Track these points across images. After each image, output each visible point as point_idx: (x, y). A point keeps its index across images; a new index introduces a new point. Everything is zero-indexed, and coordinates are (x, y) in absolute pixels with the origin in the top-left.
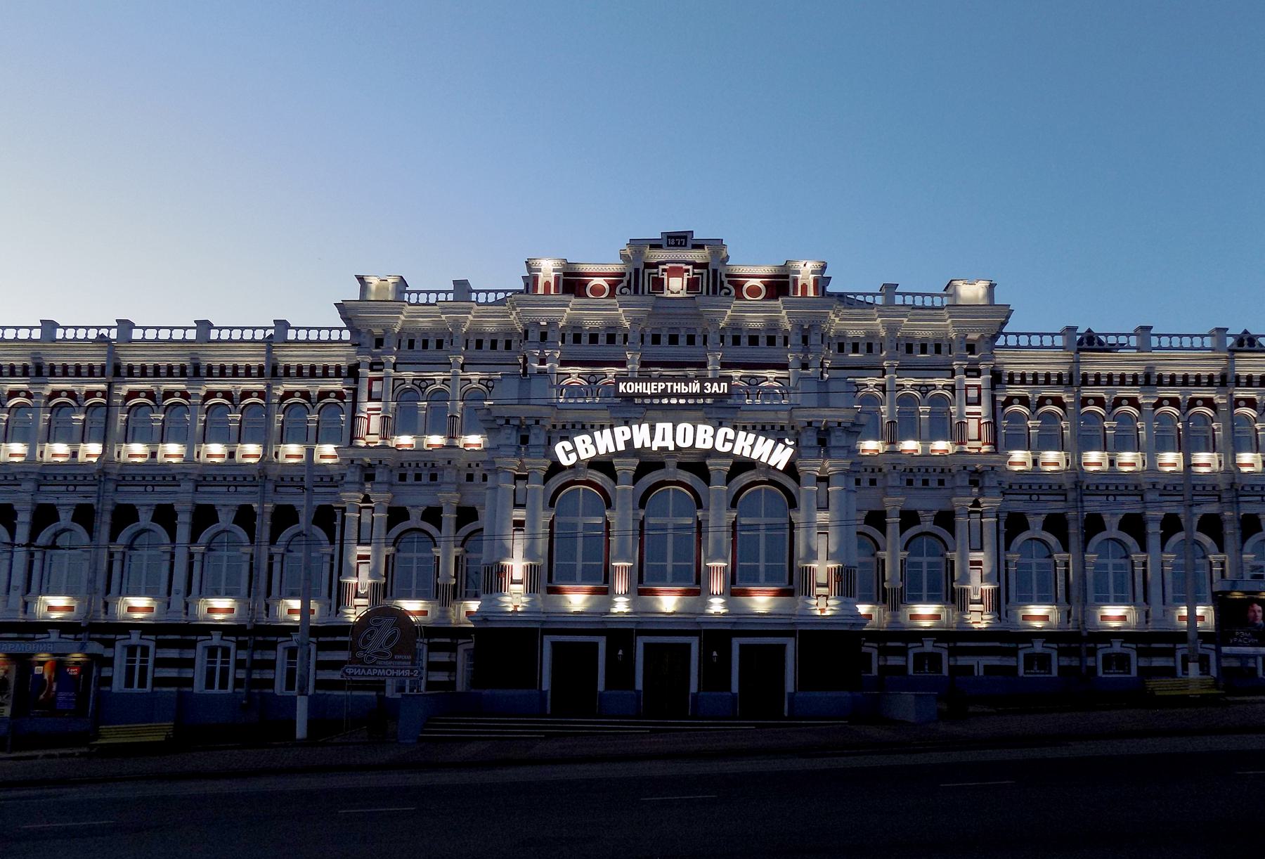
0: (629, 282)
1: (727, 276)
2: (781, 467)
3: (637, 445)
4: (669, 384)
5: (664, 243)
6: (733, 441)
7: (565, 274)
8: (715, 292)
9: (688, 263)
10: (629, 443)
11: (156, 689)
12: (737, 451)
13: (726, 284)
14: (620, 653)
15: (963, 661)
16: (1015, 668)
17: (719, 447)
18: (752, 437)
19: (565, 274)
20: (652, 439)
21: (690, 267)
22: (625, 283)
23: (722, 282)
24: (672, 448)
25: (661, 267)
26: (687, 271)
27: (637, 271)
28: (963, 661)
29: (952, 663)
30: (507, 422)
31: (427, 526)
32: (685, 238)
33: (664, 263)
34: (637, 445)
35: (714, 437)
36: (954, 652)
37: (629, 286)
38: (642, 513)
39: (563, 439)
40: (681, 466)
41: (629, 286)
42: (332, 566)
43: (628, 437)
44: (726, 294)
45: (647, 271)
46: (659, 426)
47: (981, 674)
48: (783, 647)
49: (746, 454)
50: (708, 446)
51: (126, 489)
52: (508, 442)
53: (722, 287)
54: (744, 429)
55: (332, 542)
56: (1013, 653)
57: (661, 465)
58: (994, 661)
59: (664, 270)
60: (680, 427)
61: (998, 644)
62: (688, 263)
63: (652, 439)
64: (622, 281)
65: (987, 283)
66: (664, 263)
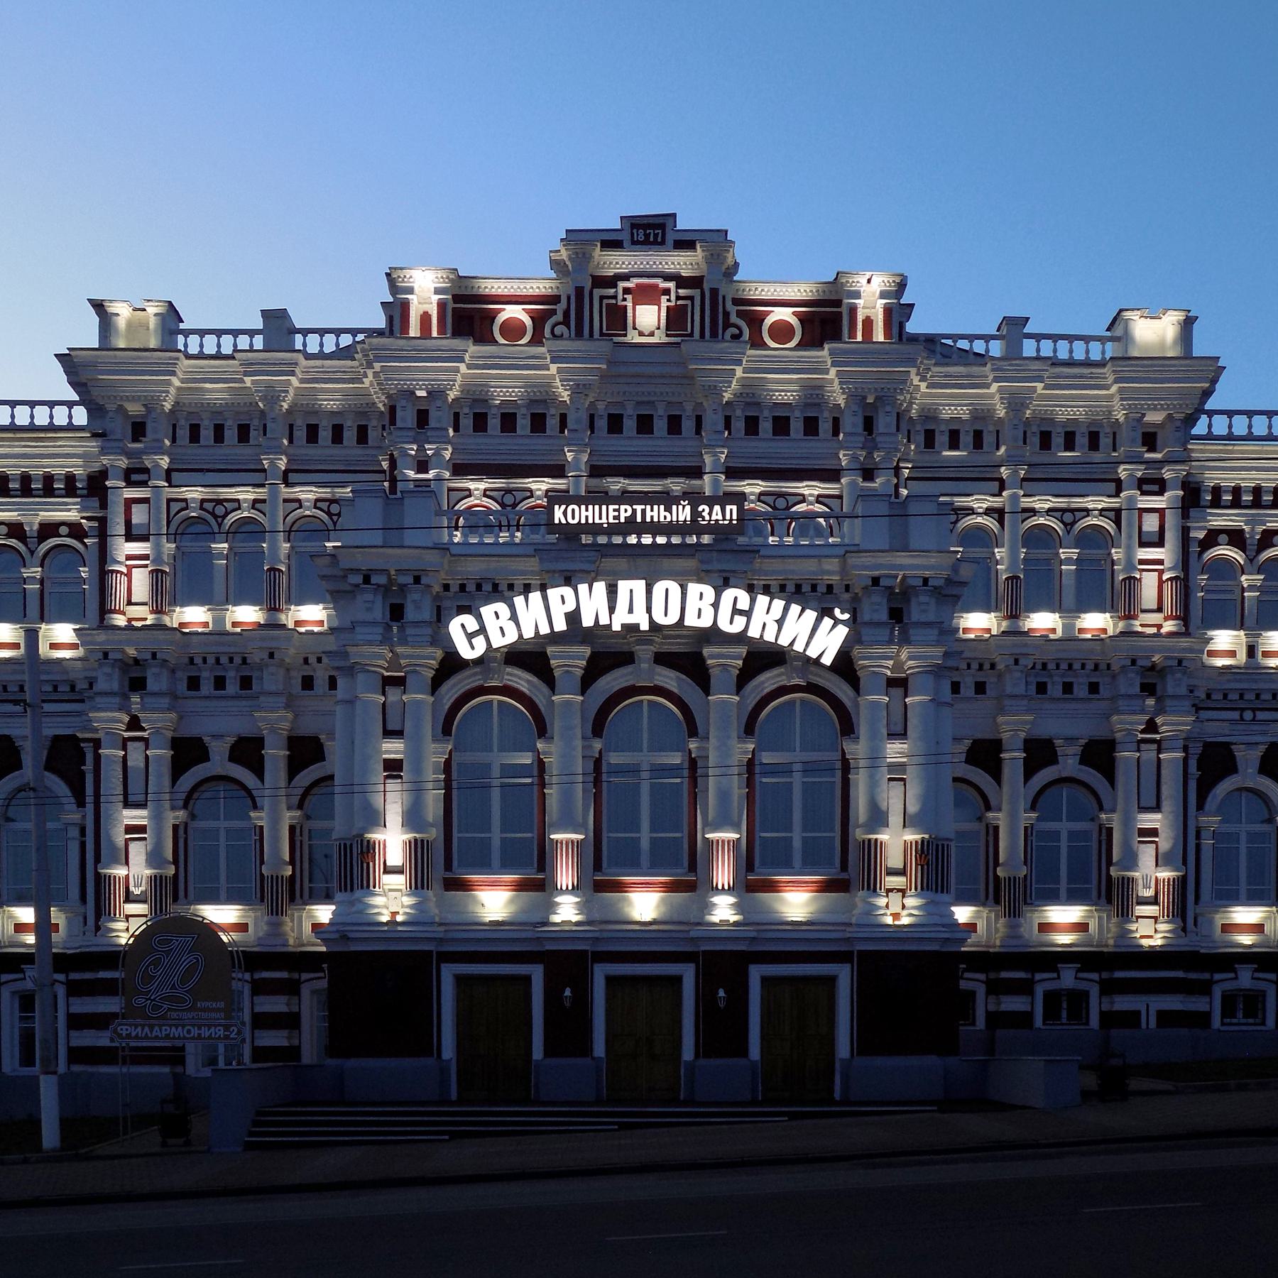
0: (566, 314)
2: (827, 660)
3: (587, 622)
4: (639, 508)
5: (625, 237)
6: (748, 614)
8: (714, 334)
9: (667, 277)
10: (573, 617)
11: (76, 1068)
12: (754, 632)
13: (734, 319)
14: (568, 992)
15: (1123, 1003)
17: (724, 626)
18: (779, 604)
20: (612, 610)
21: (671, 285)
22: (559, 317)
23: (727, 315)
24: (645, 626)
25: (622, 285)
26: (667, 292)
28: (1123, 1003)
29: (991, 1008)
30: (367, 580)
31: (1092, 776)
32: (662, 227)
33: (626, 277)
34: (587, 622)
35: (716, 605)
36: (1109, 988)
37: (566, 322)
38: (597, 745)
39: (462, 610)
40: (663, 659)
41: (566, 322)
42: (83, 845)
43: (570, 606)
44: (736, 337)
45: (598, 292)
46: (624, 586)
47: (1153, 1024)
48: (831, 981)
49: (770, 637)
50: (706, 622)
52: (369, 617)
53: (727, 325)
54: (766, 590)
55: (81, 803)
56: (1204, 989)
57: (627, 658)
58: (1173, 1003)
60: (659, 588)
61: (1180, 974)
62: (667, 277)
63: (612, 610)
64: (554, 312)
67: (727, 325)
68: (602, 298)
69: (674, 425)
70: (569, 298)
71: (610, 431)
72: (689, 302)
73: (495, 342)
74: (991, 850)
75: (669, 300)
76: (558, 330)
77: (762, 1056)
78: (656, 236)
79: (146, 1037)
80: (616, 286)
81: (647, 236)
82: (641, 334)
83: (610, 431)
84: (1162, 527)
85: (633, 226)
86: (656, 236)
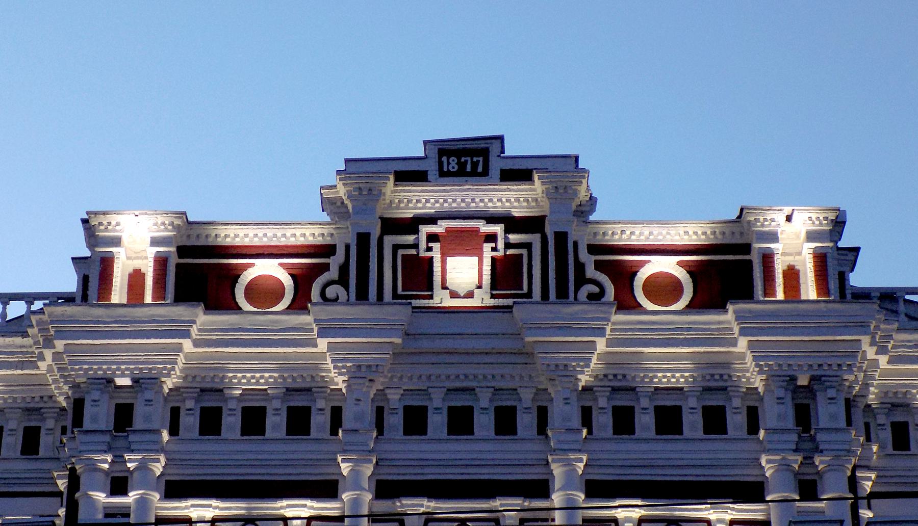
0: (344, 269)
8: (562, 293)
16: (507, 231)
22: (333, 273)
23: (580, 267)
26: (491, 238)
27: (363, 239)
33: (432, 220)
37: (343, 280)
45: (390, 240)
53: (581, 280)
59: (432, 238)
62: (492, 219)
64: (325, 268)
66: (432, 220)
68: (396, 247)
70: (348, 247)
73: (237, 308)
76: (331, 292)
78: (475, 165)
80: (416, 232)
81: (462, 166)
82: (454, 295)
86: (475, 165)
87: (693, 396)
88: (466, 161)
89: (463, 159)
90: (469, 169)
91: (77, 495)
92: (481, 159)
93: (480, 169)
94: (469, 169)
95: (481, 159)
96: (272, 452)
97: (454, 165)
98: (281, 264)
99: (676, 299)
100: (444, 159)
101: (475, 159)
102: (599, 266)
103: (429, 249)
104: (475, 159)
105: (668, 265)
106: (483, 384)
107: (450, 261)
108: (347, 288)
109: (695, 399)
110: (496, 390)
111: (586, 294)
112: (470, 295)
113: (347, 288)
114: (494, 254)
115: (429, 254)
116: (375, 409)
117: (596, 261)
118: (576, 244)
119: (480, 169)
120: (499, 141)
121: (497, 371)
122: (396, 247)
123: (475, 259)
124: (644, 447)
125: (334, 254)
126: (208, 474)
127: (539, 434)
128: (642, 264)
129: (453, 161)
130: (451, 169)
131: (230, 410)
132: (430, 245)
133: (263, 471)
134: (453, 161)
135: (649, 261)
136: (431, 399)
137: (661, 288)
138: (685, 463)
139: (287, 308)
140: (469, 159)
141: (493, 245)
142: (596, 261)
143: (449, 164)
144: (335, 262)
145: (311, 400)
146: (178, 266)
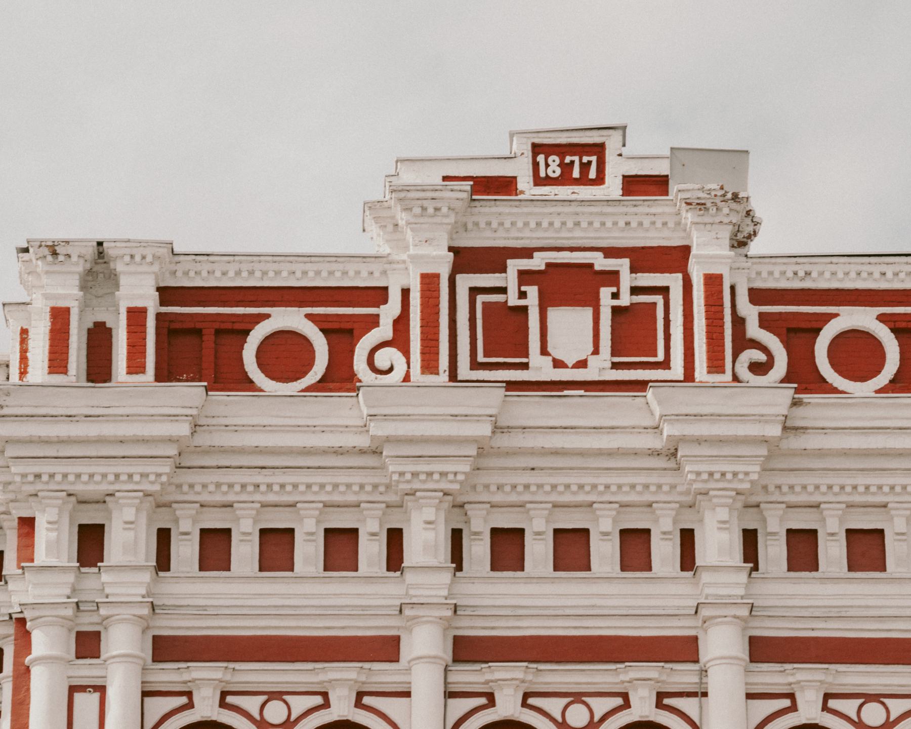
0: (401, 323)
1: (757, 296)
7: (167, 294)
8: (716, 365)
13: (754, 330)
16: (634, 270)
19: (167, 294)
22: (385, 331)
23: (739, 323)
26: (612, 277)
27: (429, 282)
32: (599, 149)
33: (527, 253)
37: (400, 340)
44: (758, 368)
45: (465, 282)
51: (189, 412)
53: (742, 342)
59: (525, 277)
60: (551, 159)
62: (610, 252)
64: (373, 322)
65: (755, 247)
66: (527, 253)
67: (742, 342)
68: (474, 291)
69: (635, 547)
70: (406, 293)
71: (496, 565)
72: (661, 357)
73: (248, 384)
74: (644, 612)
75: (615, 296)
76: (384, 358)
77: (598, 293)
78: (585, 167)
79: (577, 697)
80: (503, 269)
81: (567, 168)
82: (558, 364)
83: (496, 565)
84: (136, 537)
85: (537, 149)
86: (585, 167)
87: (129, 505)
88: (572, 162)
89: (568, 159)
90: (576, 174)
91: (27, 660)
92: (594, 159)
93: (592, 174)
94: (576, 174)
95: (594, 159)
96: (305, 596)
97: (555, 170)
98: (309, 316)
99: (877, 370)
100: (541, 158)
101: (585, 159)
102: (765, 321)
103: (523, 295)
104: (568, 159)
105: (864, 318)
106: (607, 498)
107: (555, 315)
108: (406, 353)
109: (904, 520)
110: (622, 506)
111: (746, 365)
112: (582, 364)
113: (406, 353)
114: (616, 303)
115: (522, 302)
116: (76, 530)
117: (437, 276)
118: (733, 288)
119: (592, 174)
120: (620, 132)
121: (588, 480)
122: (474, 291)
123: (588, 312)
124: (831, 588)
125: (385, 301)
126: (213, 628)
127: (683, 568)
128: (828, 318)
129: (554, 160)
130: (551, 175)
131: (244, 534)
132: (523, 288)
133: (321, 623)
134: (554, 160)
135: (836, 315)
136: (764, 520)
137: (856, 354)
138: (889, 612)
139: (320, 381)
140: (576, 159)
141: (614, 290)
142: (437, 276)
143: (547, 165)
144: (389, 312)
145: (359, 521)
146: (159, 316)
